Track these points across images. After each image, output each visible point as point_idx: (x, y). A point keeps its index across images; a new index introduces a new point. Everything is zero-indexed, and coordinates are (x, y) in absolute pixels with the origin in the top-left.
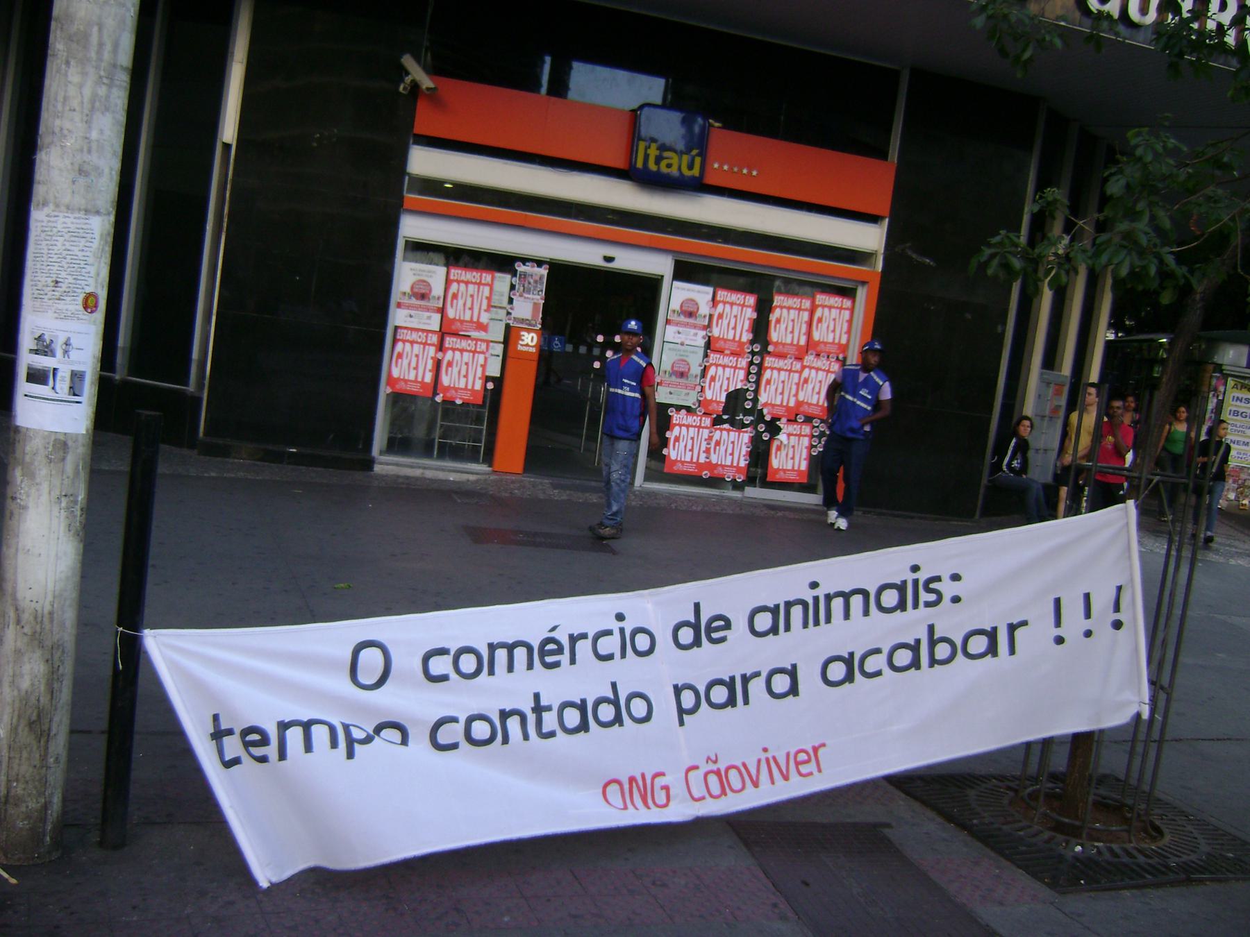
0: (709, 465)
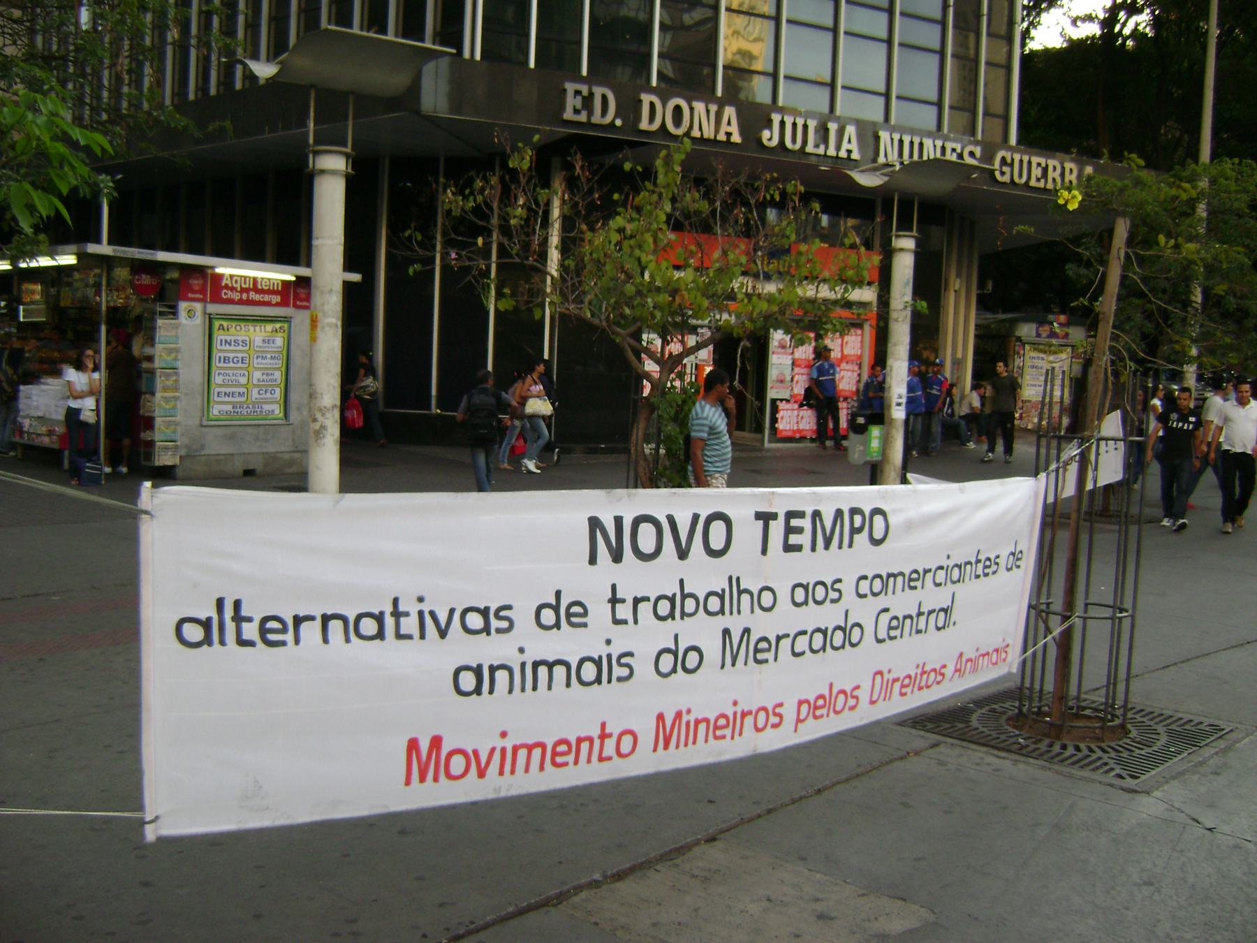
0: (799, 431)
